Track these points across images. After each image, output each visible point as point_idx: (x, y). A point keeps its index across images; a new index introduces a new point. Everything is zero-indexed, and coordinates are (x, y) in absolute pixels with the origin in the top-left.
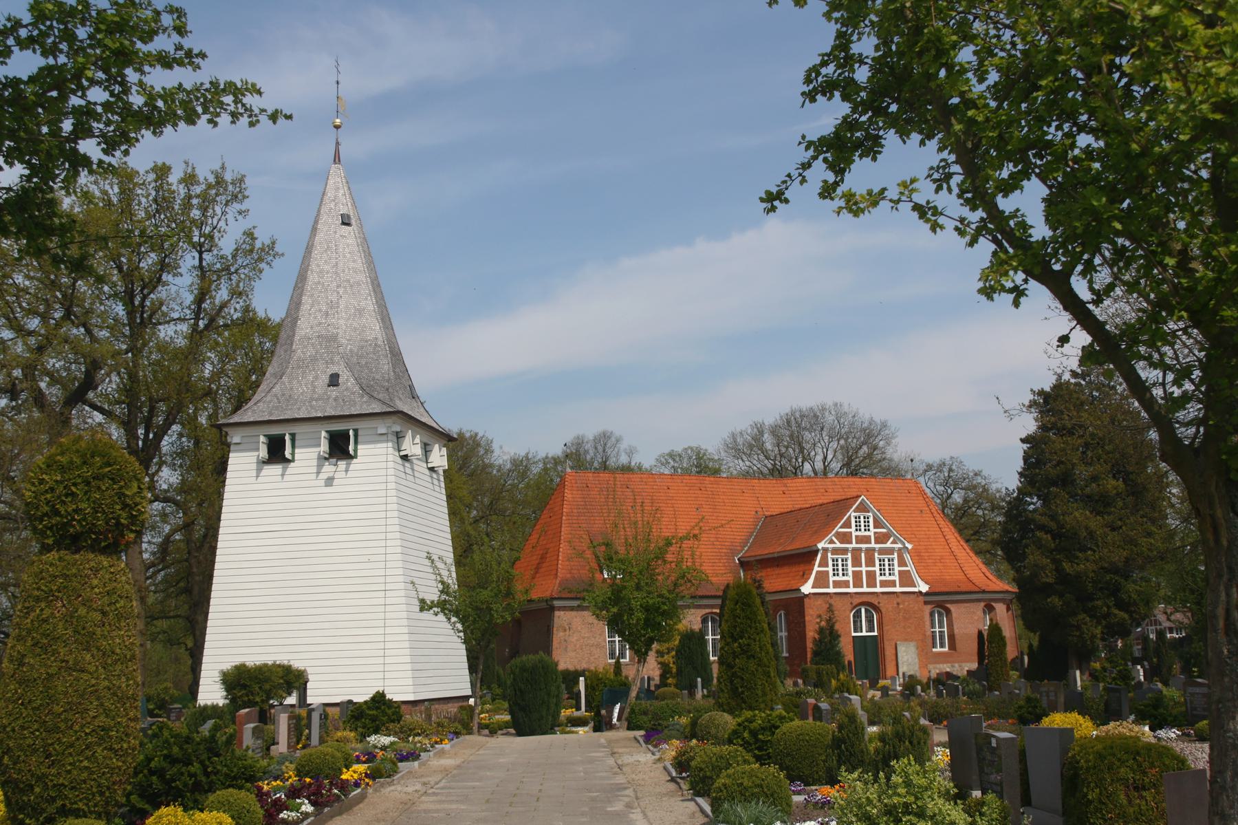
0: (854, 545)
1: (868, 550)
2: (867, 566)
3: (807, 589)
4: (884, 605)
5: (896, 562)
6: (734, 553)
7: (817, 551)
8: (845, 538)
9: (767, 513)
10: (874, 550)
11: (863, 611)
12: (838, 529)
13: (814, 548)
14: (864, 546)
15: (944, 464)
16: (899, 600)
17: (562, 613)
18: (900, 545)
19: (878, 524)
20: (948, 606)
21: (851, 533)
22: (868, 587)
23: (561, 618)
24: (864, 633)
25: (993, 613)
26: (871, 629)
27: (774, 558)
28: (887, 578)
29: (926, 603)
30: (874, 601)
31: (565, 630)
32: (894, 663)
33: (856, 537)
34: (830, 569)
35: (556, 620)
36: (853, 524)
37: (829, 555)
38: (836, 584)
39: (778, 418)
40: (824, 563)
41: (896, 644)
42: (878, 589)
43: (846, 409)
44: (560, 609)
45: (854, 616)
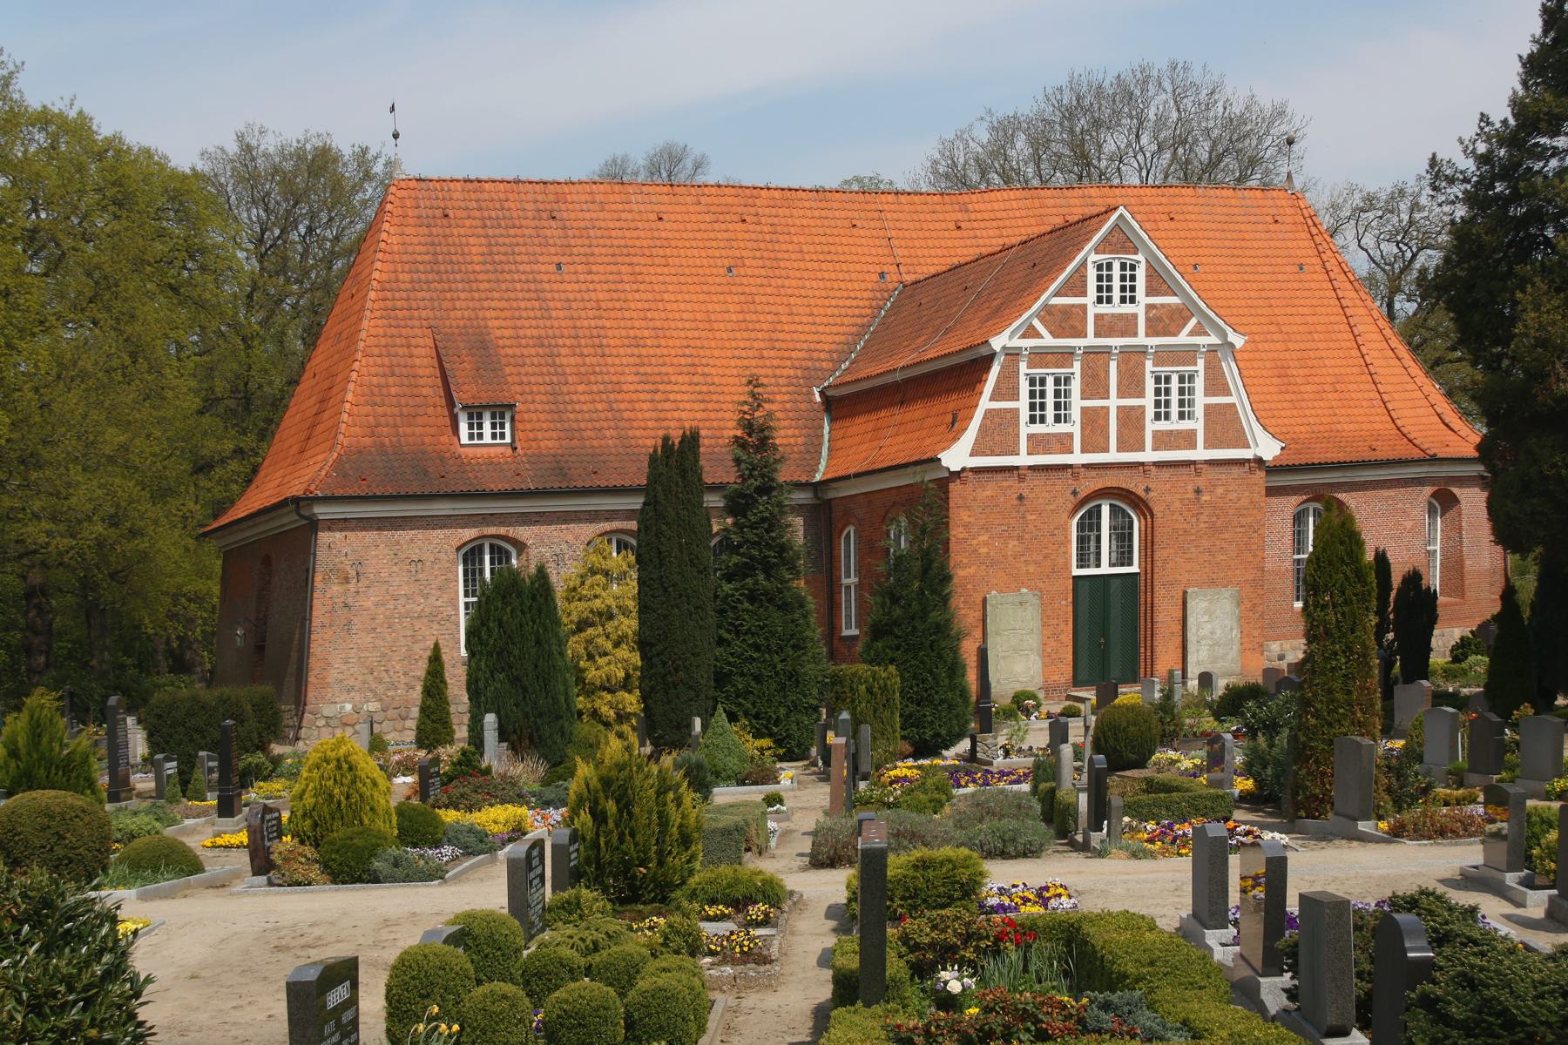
0: (1091, 340)
1: (1125, 351)
2: (1121, 395)
3: (956, 457)
4: (1164, 496)
5: (1199, 384)
6: (810, 381)
7: (992, 357)
8: (1068, 322)
9: (909, 278)
10: (1142, 351)
11: (1105, 510)
12: (1049, 296)
13: (984, 351)
14: (1116, 342)
15: (1402, 193)
16: (1201, 482)
17: (338, 535)
18: (1214, 339)
19: (1158, 283)
20: (1342, 496)
21: (1084, 308)
22: (1121, 448)
23: (333, 548)
24: (1105, 569)
25: (1452, 513)
26: (1124, 557)
27: (896, 384)
28: (1174, 424)
29: (1271, 492)
30: (1136, 484)
31: (347, 580)
32: (1178, 640)
33: (1098, 317)
34: (1023, 404)
35: (321, 554)
37: (1023, 368)
38: (1038, 444)
39: (1041, 97)
40: (1007, 390)
41: (1185, 593)
42: (1149, 455)
43: (1196, 75)
44: (332, 525)
45: (1081, 526)
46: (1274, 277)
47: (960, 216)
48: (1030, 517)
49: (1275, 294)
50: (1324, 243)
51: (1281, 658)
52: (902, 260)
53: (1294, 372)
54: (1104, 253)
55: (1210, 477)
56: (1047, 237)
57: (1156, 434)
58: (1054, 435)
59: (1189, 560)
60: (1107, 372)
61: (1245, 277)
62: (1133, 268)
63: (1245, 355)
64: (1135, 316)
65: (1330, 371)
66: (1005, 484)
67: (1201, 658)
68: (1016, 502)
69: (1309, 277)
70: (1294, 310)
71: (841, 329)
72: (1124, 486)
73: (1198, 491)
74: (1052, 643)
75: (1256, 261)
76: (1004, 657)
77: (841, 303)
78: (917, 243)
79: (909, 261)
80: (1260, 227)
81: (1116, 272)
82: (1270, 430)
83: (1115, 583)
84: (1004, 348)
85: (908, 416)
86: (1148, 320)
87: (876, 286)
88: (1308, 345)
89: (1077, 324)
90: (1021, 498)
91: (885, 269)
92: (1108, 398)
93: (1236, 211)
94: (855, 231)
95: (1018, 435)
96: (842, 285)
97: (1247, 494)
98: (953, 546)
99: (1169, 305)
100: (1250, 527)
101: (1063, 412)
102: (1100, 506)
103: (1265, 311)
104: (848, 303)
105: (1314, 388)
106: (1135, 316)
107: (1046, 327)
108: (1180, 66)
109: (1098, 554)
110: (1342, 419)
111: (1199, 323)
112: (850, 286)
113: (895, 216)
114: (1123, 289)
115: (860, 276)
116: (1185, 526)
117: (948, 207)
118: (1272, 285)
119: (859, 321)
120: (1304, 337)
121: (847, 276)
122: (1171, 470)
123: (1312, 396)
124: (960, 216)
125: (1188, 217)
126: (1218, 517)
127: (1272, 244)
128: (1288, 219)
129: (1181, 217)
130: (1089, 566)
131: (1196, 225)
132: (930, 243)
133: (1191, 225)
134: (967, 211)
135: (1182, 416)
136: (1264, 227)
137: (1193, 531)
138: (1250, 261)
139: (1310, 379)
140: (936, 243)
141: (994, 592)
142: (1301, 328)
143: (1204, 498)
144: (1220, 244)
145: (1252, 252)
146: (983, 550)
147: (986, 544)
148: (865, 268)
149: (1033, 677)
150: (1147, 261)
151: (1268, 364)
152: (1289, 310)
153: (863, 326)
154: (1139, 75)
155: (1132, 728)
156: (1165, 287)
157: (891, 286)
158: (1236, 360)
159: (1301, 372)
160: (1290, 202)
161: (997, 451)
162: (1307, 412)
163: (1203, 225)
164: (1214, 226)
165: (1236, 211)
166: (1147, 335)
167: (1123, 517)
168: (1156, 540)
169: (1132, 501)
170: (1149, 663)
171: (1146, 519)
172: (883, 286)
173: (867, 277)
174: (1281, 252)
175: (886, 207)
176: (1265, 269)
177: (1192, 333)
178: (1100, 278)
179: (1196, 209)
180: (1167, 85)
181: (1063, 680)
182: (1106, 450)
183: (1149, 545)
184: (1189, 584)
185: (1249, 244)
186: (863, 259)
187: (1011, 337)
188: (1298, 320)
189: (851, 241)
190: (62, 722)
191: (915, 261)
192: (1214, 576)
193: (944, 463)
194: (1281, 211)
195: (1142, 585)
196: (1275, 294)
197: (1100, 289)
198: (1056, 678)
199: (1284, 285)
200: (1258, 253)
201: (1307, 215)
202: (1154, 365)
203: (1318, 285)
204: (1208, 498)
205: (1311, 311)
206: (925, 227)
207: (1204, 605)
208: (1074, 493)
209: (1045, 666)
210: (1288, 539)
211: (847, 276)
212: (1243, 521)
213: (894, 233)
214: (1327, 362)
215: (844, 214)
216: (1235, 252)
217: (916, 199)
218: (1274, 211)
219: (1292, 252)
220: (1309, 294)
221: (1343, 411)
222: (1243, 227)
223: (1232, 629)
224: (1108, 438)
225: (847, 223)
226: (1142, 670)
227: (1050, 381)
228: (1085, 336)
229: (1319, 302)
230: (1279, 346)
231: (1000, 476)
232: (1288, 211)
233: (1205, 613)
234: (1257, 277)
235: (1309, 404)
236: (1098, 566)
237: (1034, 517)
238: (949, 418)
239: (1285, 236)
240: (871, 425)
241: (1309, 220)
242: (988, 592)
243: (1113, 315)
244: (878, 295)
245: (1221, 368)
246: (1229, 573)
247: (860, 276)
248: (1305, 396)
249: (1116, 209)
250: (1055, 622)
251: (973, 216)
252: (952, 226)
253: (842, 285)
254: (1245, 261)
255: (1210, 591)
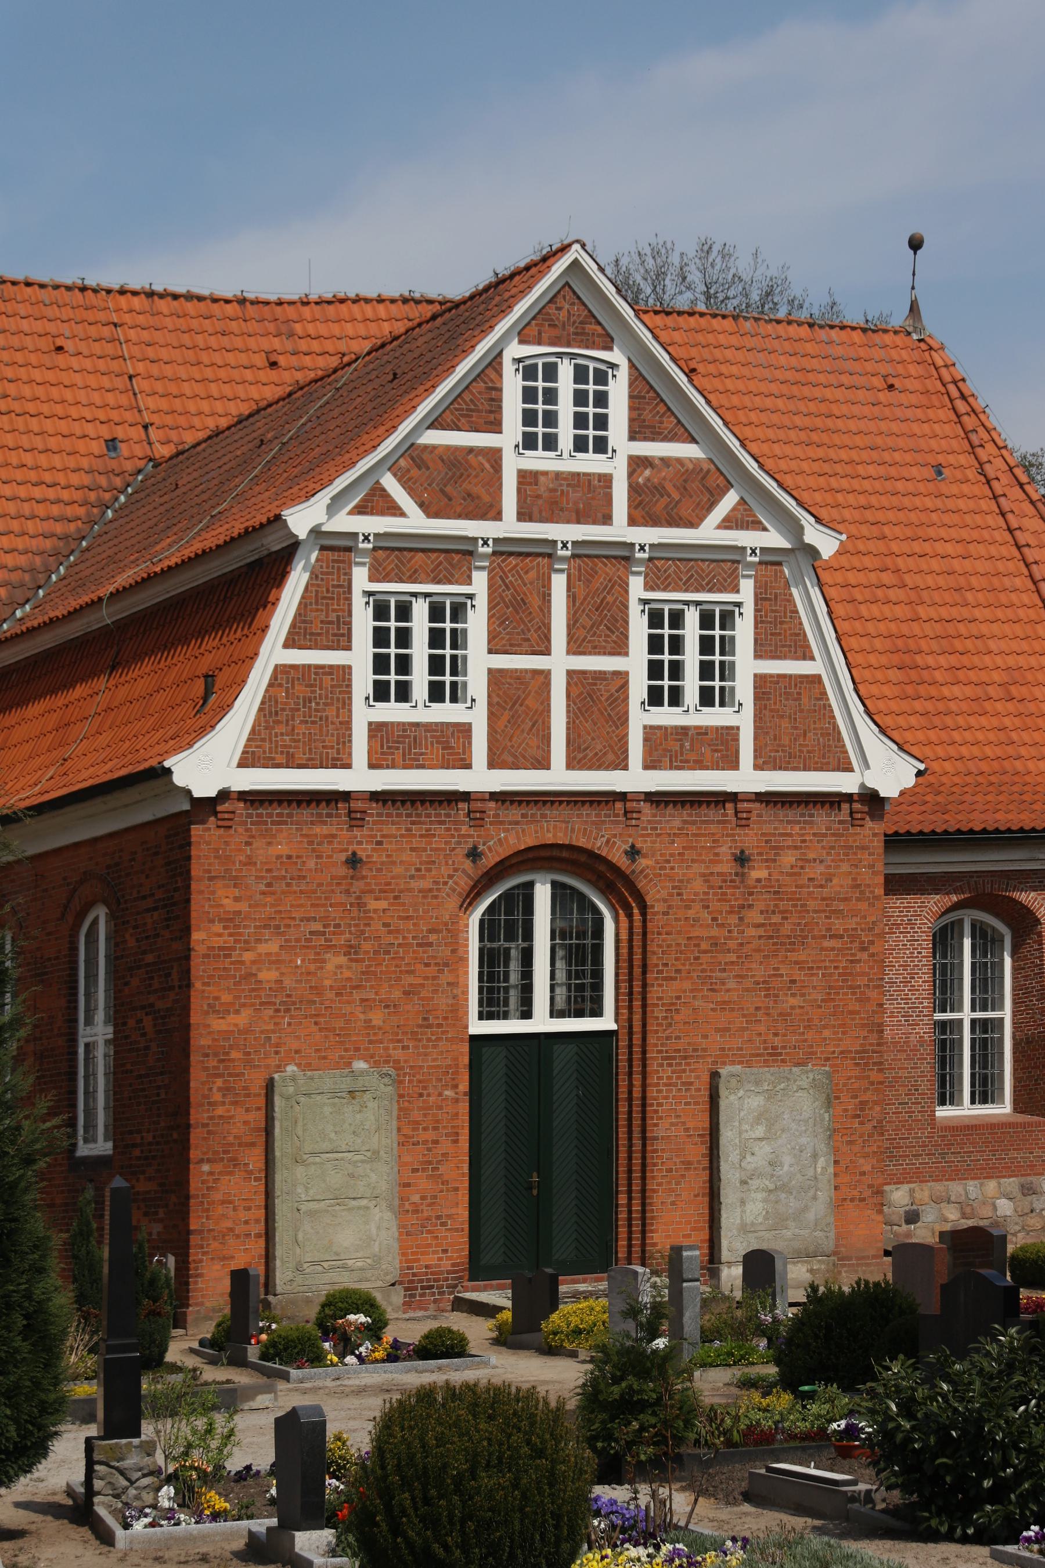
2: (575, 647)
5: (744, 631)
7: (292, 548)
9: (164, 451)
11: (543, 895)
13: (274, 543)
16: (749, 840)
18: (774, 539)
21: (494, 456)
29: (896, 885)
33: (526, 478)
36: (512, 406)
37: (360, 579)
41: (715, 1075)
43: (742, 264)
45: (487, 928)
46: (888, 485)
47: (276, 343)
48: (373, 904)
49: (891, 515)
50: (981, 430)
51: (912, 1218)
52: (156, 419)
53: (930, 660)
54: (539, 343)
55: (767, 828)
56: (425, 327)
57: (651, 733)
58: (429, 727)
59: (724, 1006)
60: (546, 598)
61: (834, 483)
62: (601, 378)
63: (839, 577)
64: (606, 480)
65: (999, 660)
66: (319, 830)
67: (749, 1218)
68: (343, 871)
69: (954, 489)
70: (927, 547)
71: (20, 543)
72: (582, 842)
73: (742, 859)
74: (423, 1182)
75: (854, 455)
76: (311, 1213)
77: (22, 492)
78: (187, 388)
79: (169, 420)
80: (861, 395)
81: (566, 383)
82: (895, 735)
83: (562, 1054)
84: (316, 532)
85: (123, 692)
86: (634, 489)
87: (98, 464)
88: (955, 612)
89: (478, 490)
90: (354, 861)
91: (120, 432)
92: (547, 652)
93: (815, 363)
94: (60, 359)
95: (347, 724)
96: (28, 459)
97: (845, 867)
98: (199, 968)
99: (679, 460)
100: (853, 938)
101: (448, 678)
102: (530, 885)
103: (871, 546)
104: (37, 492)
105: (969, 691)
106: (606, 480)
107: (411, 492)
108: (716, 249)
109: (527, 990)
110: (1023, 751)
111: (743, 501)
112: (43, 460)
113: (145, 335)
114: (580, 421)
115: (67, 444)
116: (715, 932)
117: (252, 327)
118: (884, 501)
119: (59, 528)
120: (948, 597)
121: (38, 442)
122: (685, 813)
123: (964, 706)
124: (276, 343)
125: (723, 369)
126: (785, 914)
127: (883, 426)
128: (912, 384)
129: (711, 368)
130: (506, 1016)
131: (740, 385)
132: (214, 389)
133: (730, 384)
134: (291, 335)
135: (706, 698)
136: (870, 396)
137: (732, 944)
138: (844, 455)
139: (961, 675)
140: (227, 390)
141: (291, 1068)
142: (941, 581)
143: (755, 874)
144: (786, 420)
145: (846, 439)
146: (268, 975)
147: (276, 962)
148: (77, 428)
149: (377, 1259)
150: (632, 365)
151: (878, 644)
152: (917, 547)
153: (65, 538)
154: (650, 263)
155: (486, 1480)
156: (669, 423)
157: (129, 466)
158: (820, 585)
159: (942, 660)
160: (916, 355)
161: (301, 756)
162: (956, 736)
163: (752, 386)
164: (774, 388)
165: (815, 363)
166: (632, 522)
167: (581, 910)
168: (652, 960)
169: (601, 876)
170: (636, 1229)
171: (630, 916)
172: (113, 464)
173: (81, 446)
174: (901, 442)
175: (127, 318)
176: (872, 470)
177: (728, 523)
178: (529, 395)
179: (740, 356)
180: (695, 276)
181: (446, 1265)
182: (543, 763)
183: (637, 971)
184: (725, 1056)
185: (840, 424)
186: (74, 412)
187: (333, 508)
188: (935, 564)
189: (50, 376)
190: (56, 1254)
191: (182, 421)
192: (777, 1041)
193: (179, 779)
194: (900, 369)
195: (623, 1058)
196: (891, 515)
197: (529, 418)
198: (431, 1259)
199: (906, 502)
200: (858, 440)
201: (947, 378)
202: (648, 587)
203: (971, 504)
204: (763, 874)
205: (959, 549)
206: (206, 360)
207: (755, 1102)
208: (474, 854)
209: (405, 1233)
210: (924, 981)
211: (38, 442)
212: (838, 925)
213: (141, 367)
214: (992, 645)
215: (39, 326)
216: (815, 437)
217: (190, 307)
218: (889, 369)
219: (922, 443)
220: (955, 518)
221: (1026, 736)
222: (828, 393)
223: (815, 1156)
224: (547, 739)
225: (44, 344)
226: (623, 1243)
227: (420, 610)
228: (498, 516)
229: (975, 534)
230: (899, 611)
231: (306, 813)
232: (913, 370)
233: (757, 1121)
234: (856, 484)
235: (960, 721)
236: (527, 1014)
237: (383, 904)
238: (199, 686)
239: (909, 413)
240: (54, 719)
241: (952, 388)
242: (279, 1068)
243: (558, 475)
244: (103, 481)
245: (790, 599)
246: (810, 1035)
247: (67, 444)
248: (952, 705)
249: (564, 249)
250: (431, 1135)
251: (303, 345)
252: (260, 360)
253: (28, 459)
254: (832, 454)
255: (767, 1073)
